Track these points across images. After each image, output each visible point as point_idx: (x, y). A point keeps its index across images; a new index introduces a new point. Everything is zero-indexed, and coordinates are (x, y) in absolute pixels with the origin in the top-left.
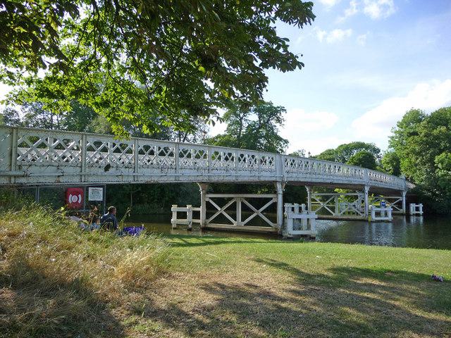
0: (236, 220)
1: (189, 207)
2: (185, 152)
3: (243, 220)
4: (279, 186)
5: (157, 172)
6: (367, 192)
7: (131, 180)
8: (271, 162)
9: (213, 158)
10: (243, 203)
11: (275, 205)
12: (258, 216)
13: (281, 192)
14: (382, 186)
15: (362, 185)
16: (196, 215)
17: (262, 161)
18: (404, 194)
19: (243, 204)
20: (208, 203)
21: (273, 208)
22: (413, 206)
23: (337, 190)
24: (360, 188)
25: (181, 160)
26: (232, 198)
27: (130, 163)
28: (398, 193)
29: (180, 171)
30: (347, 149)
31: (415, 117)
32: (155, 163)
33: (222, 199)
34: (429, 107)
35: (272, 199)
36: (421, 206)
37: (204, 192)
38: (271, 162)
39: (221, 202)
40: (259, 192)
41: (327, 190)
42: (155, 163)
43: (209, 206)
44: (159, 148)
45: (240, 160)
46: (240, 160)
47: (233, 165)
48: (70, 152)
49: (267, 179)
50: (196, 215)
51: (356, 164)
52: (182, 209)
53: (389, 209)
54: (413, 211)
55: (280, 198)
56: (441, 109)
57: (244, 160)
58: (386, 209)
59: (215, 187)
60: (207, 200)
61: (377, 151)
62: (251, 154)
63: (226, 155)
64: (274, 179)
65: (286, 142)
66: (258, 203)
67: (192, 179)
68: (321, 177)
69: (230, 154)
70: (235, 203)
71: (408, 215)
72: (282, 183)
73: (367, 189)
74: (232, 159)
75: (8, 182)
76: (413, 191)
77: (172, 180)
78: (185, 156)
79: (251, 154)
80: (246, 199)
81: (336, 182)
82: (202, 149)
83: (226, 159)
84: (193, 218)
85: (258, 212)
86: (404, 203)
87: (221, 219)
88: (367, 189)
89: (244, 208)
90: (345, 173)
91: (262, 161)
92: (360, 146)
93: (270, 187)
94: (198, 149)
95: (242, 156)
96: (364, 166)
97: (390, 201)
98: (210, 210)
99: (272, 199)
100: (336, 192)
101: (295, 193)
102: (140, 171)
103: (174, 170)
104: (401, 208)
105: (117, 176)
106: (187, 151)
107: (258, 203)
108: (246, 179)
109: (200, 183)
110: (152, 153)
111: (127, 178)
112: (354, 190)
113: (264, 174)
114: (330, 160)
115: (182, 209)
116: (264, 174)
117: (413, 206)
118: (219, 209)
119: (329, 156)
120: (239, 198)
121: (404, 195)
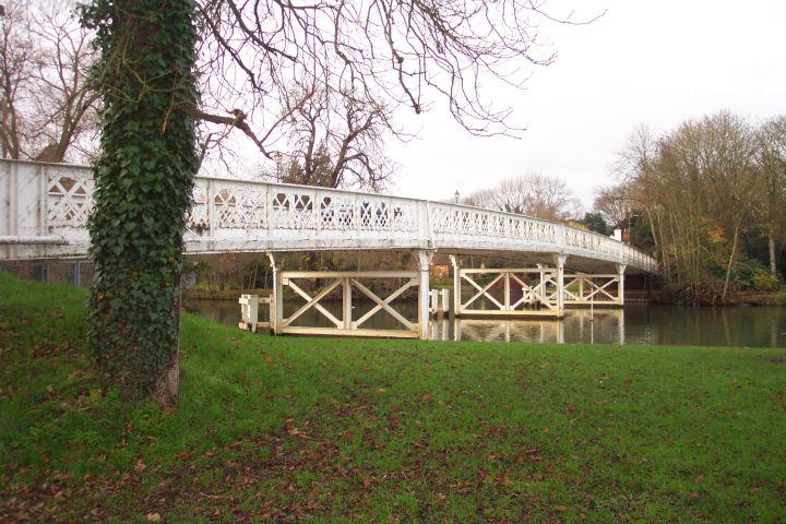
0: (341, 319)
2: (306, 202)
3: (512, 304)
6: (561, 266)
11: (416, 289)
12: (383, 311)
19: (355, 291)
24: (548, 259)
26: (498, 274)
28: (611, 267)
33: (599, 279)
39: (313, 286)
40: (483, 266)
44: (296, 198)
50: (263, 313)
56: (691, 136)
59: (290, 260)
60: (285, 282)
62: (301, 193)
63: (300, 199)
66: (383, 289)
67: (261, 248)
69: (306, 199)
70: (340, 288)
72: (427, 252)
75: (36, 255)
79: (301, 193)
80: (365, 281)
83: (299, 207)
85: (383, 304)
88: (561, 262)
93: (406, 257)
95: (328, 201)
96: (592, 229)
99: (409, 279)
107: (383, 289)
111: (587, 253)
118: (487, 295)
120: (506, 274)
121: (622, 272)
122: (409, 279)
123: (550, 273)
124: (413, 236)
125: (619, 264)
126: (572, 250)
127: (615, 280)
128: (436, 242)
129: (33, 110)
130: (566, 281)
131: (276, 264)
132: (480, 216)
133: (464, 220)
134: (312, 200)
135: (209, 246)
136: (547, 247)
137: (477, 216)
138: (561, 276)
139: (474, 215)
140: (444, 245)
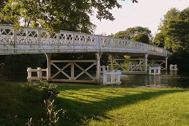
0: (70, 77)
1: (39, 69)
2: (44, 35)
3: (75, 76)
4: (98, 55)
5: (28, 47)
7: (13, 53)
8: (93, 40)
9: (61, 38)
10: (75, 66)
11: (96, 65)
13: (99, 59)
14: (155, 54)
15: (143, 54)
16: (44, 73)
17: (88, 40)
18: (167, 59)
20: (52, 66)
21: (94, 69)
22: (171, 66)
23: (125, 56)
24: (142, 56)
25: (42, 39)
26: (68, 63)
27: (12, 42)
28: (163, 58)
29: (41, 46)
30: (133, 30)
31: (174, 12)
32: (26, 41)
34: (181, 8)
35: (93, 63)
36: (176, 66)
37: (49, 59)
38: (93, 40)
39: (61, 65)
41: (120, 56)
42: (26, 41)
43: (52, 68)
44: (67, 35)
45: (61, 38)
46: (76, 39)
47: (72, 42)
48: (9, 36)
49: (91, 51)
50: (44, 73)
51: (137, 40)
52: (34, 70)
53: (159, 68)
54: (171, 69)
55: (99, 62)
57: (78, 39)
58: (157, 68)
59: (54, 56)
61: (149, 32)
62: (68, 34)
63: (68, 36)
64: (95, 51)
65: (95, 26)
66: (85, 66)
68: (121, 49)
69: (70, 36)
71: (168, 71)
73: (146, 56)
74: (71, 39)
76: (172, 56)
77: (37, 52)
78: (44, 37)
79: (82, 35)
81: (130, 52)
82: (33, 30)
83: (68, 38)
84: (61, 72)
86: (167, 64)
87: (61, 76)
88: (146, 56)
89: (76, 68)
90: (133, 47)
91: (88, 40)
92: (140, 29)
93: (92, 55)
94: (31, 30)
96: (143, 42)
97: (159, 63)
98: (53, 70)
100: (125, 58)
101: (105, 58)
102: (18, 47)
103: (37, 46)
104: (165, 67)
105: (4, 50)
106: (10, 30)
108: (79, 51)
109: (47, 54)
110: (24, 35)
111: (155, 54)
112: (136, 57)
113: (89, 47)
114: (120, 37)
115: (34, 70)
116: (89, 47)
117: (171, 66)
118: (60, 69)
119: (121, 36)
120: (72, 63)
121: (167, 60)
122: (93, 63)
123: (143, 60)
124: (95, 48)
125: (165, 57)
126: (149, 52)
127: (165, 62)
128: (102, 50)
129: (160, 31)
130: (148, 63)
131: (48, 58)
132: (124, 42)
133: (126, 44)
134: (72, 36)
135: (39, 51)
136: (35, 50)
137: (124, 42)
138: (146, 60)
139: (123, 41)
140: (105, 51)
